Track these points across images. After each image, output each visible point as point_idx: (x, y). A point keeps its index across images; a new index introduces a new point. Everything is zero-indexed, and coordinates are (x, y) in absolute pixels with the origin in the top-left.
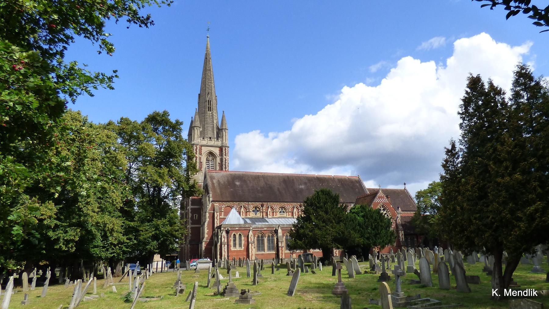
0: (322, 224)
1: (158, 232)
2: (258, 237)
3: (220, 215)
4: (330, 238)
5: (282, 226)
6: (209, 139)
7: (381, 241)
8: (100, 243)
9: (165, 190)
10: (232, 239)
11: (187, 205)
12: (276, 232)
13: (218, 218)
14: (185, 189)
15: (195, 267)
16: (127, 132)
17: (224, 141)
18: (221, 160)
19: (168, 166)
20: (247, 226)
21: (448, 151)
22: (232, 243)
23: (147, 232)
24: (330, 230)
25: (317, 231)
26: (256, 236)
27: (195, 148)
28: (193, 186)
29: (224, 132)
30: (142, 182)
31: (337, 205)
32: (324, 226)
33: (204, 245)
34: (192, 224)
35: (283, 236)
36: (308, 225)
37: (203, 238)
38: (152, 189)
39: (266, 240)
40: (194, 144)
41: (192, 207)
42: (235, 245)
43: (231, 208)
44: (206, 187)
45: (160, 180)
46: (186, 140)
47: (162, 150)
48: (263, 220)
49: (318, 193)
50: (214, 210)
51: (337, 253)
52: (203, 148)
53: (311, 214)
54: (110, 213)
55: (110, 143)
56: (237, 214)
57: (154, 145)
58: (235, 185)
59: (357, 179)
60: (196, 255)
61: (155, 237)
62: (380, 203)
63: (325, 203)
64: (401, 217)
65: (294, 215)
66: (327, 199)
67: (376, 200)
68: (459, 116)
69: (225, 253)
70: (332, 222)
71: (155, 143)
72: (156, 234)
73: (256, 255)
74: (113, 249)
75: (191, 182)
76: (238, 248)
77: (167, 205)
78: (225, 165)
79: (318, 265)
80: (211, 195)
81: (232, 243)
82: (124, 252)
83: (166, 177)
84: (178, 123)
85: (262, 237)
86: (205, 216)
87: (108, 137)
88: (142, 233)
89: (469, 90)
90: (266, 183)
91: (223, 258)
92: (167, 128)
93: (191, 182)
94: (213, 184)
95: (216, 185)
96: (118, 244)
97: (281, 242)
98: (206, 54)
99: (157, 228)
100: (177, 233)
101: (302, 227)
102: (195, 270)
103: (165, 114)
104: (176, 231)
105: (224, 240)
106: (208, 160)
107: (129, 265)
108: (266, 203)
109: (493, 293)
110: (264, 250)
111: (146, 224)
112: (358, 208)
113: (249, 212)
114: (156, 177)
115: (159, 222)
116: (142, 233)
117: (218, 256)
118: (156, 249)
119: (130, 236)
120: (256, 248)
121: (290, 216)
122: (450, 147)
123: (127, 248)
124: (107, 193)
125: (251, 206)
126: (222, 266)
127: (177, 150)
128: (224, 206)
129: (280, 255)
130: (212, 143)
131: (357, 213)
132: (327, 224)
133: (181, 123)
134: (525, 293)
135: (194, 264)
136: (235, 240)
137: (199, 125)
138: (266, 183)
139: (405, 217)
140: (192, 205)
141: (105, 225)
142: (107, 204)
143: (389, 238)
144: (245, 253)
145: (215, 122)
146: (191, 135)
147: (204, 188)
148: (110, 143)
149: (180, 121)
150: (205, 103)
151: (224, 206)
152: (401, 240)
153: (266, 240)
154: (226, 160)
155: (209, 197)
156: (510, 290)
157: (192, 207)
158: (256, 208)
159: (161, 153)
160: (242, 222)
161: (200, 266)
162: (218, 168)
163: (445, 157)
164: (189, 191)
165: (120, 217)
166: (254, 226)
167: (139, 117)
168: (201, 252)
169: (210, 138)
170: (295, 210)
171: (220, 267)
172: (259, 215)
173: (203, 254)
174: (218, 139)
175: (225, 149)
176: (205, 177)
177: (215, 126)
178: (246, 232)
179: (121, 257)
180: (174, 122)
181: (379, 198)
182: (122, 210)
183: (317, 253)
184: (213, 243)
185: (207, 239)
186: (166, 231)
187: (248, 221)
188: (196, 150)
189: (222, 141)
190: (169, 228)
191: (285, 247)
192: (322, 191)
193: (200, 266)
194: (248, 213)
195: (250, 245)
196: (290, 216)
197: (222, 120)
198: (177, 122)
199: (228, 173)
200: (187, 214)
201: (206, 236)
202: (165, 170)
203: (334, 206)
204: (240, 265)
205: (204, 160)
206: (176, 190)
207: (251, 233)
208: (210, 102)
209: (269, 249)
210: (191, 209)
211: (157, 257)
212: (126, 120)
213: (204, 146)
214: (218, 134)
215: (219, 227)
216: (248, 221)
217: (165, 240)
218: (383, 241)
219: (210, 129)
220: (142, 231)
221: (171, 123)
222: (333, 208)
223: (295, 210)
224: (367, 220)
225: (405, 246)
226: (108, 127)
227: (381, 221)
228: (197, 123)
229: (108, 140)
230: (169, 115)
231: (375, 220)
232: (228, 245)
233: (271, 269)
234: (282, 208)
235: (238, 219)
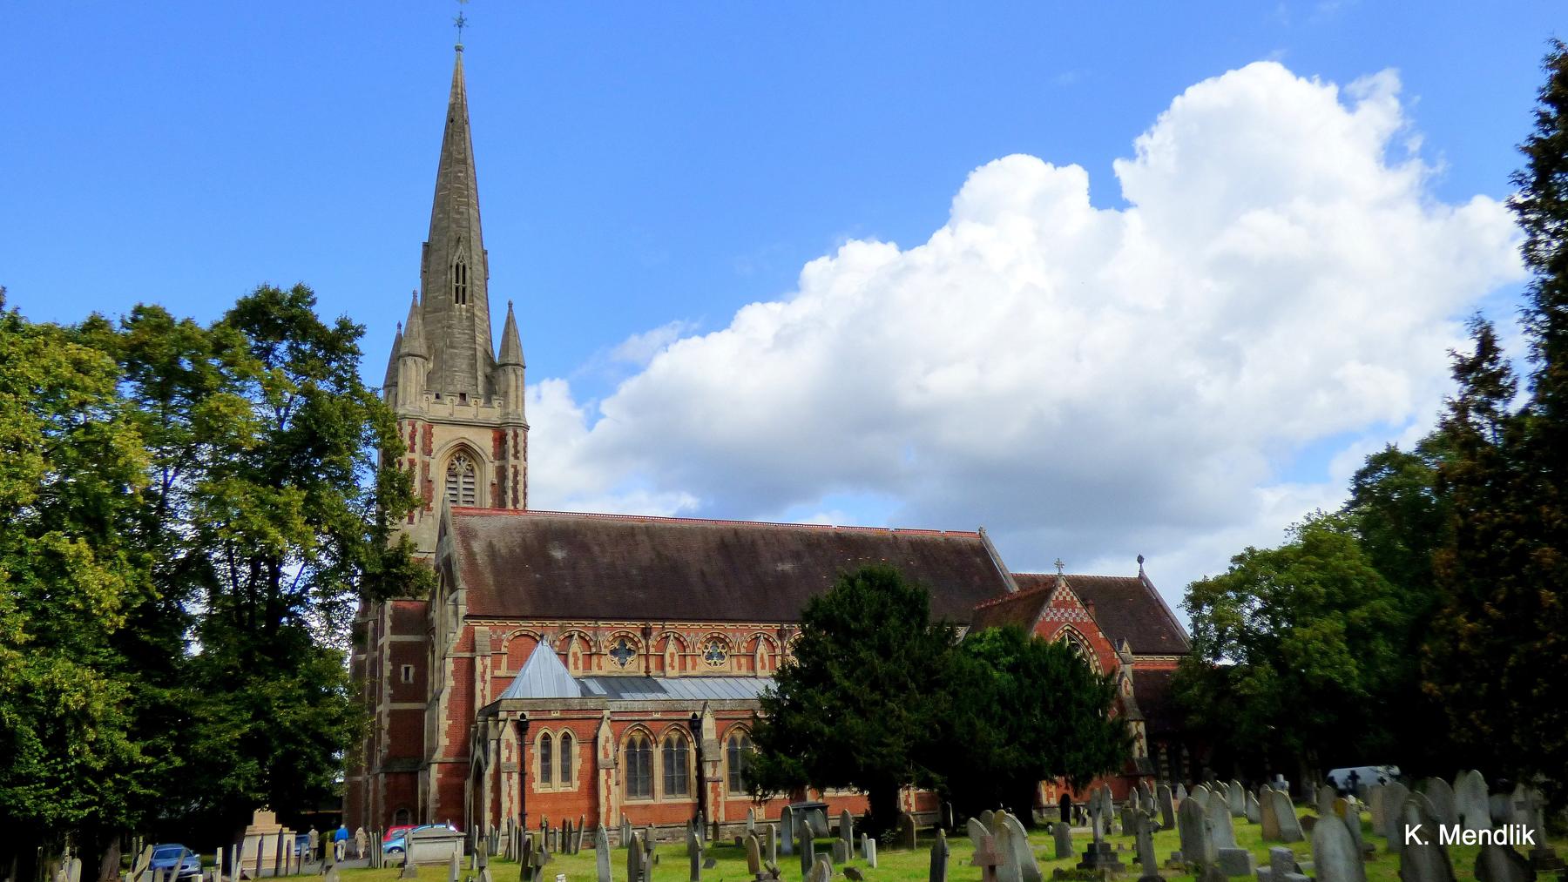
0: (866, 694)
1: (263, 724)
2: (631, 744)
4: (898, 745)
5: (717, 706)
6: (457, 400)
7: (1080, 756)
8: (35, 766)
9: (293, 572)
10: (536, 751)
11: (378, 631)
12: (695, 725)
13: (488, 677)
14: (369, 569)
15: (401, 856)
16: (155, 353)
17: (512, 407)
18: (501, 473)
19: (305, 479)
20: (591, 704)
21: (1464, 370)
22: (536, 768)
23: (222, 726)
24: (899, 718)
25: (853, 721)
26: (625, 740)
27: (407, 429)
28: (398, 558)
29: (512, 377)
30: (207, 538)
31: (921, 626)
32: (875, 703)
33: (434, 776)
34: (394, 699)
35: (720, 738)
36: (819, 698)
37: (433, 750)
38: (247, 569)
39: (658, 753)
40: (404, 417)
41: (396, 638)
42: (547, 775)
43: (536, 640)
44: (447, 565)
45: (273, 532)
46: (375, 390)
47: (286, 428)
48: (647, 683)
49: (852, 582)
50: (473, 650)
51: (912, 800)
52: (436, 430)
53: (829, 658)
54: (80, 651)
55: (85, 389)
56: (557, 661)
57: (257, 409)
58: (550, 561)
59: (975, 541)
60: (404, 808)
61: (252, 746)
62: (1059, 623)
63: (879, 618)
64: (1135, 673)
65: (759, 665)
66: (884, 605)
67: (1048, 614)
68: (1515, 215)
69: (511, 805)
70: (903, 688)
71: (258, 400)
72: (255, 731)
73: (623, 809)
74: (91, 790)
75: (393, 542)
76: (557, 785)
77: (300, 632)
78: (515, 491)
79: (858, 846)
80: (462, 595)
81: (536, 768)
82: (134, 801)
83: (298, 523)
84: (347, 331)
85: (644, 744)
86: (442, 669)
87: (79, 366)
88: (203, 730)
89: (1552, 112)
90: (659, 554)
91: (504, 820)
92: (306, 347)
93: (393, 542)
94: (470, 555)
95: (481, 559)
96: (108, 771)
97: (715, 764)
98: (452, 107)
99: (260, 709)
100: (335, 729)
101: (795, 706)
102: (402, 865)
103: (301, 295)
104: (333, 722)
105: (510, 756)
106: (452, 472)
107: (150, 848)
108: (659, 625)
109: (1408, 835)
110: (649, 791)
111: (221, 695)
112: (994, 639)
113: (599, 654)
114: (257, 521)
115: (269, 689)
116: (203, 730)
117: (488, 816)
118: (257, 790)
119: (159, 740)
120: (624, 785)
121: (744, 672)
122: (1469, 349)
123: (145, 785)
124: (64, 574)
125: (607, 632)
126: (501, 850)
127: (341, 426)
128: (509, 632)
129: (710, 809)
130: (467, 413)
131: (992, 657)
132: (885, 695)
133: (359, 332)
134: (1500, 837)
135: (399, 843)
136: (546, 758)
137: (424, 351)
138: (659, 554)
139: (1146, 674)
140: (394, 630)
141: (54, 693)
142: (70, 619)
143: (1106, 747)
144: (584, 803)
145: (480, 339)
146: (396, 384)
147: (437, 569)
148: (85, 389)
149: (355, 323)
150: (450, 270)
151: (508, 635)
152: (1136, 754)
153: (658, 753)
154: (516, 474)
155: (455, 601)
156: (1457, 828)
157: (396, 638)
158: (623, 639)
159: (279, 436)
160: (573, 691)
161: (420, 851)
162: (489, 501)
163: (1456, 390)
164: (389, 577)
165: (120, 668)
166: (615, 706)
167: (203, 304)
168: (424, 801)
169: (463, 396)
170: (762, 649)
171: (492, 854)
172: (634, 666)
173: (432, 806)
174: (489, 401)
175: (516, 435)
176: (443, 531)
177: (480, 355)
178: (588, 727)
179: (123, 819)
180: (332, 327)
181: (1058, 605)
182: (121, 640)
183: (848, 801)
184: (467, 769)
185: (446, 754)
186: (293, 722)
187: (596, 688)
188: (412, 437)
189: (506, 406)
190: (305, 711)
191: (726, 779)
192: (868, 577)
193: (420, 851)
194: (595, 659)
195: (602, 773)
196: (744, 672)
197: (506, 334)
198: (344, 326)
199: (523, 518)
200: (376, 664)
201: (444, 741)
202: (292, 495)
203: (910, 630)
204: (565, 848)
205: (439, 472)
206: (334, 571)
207: (605, 731)
208: (461, 271)
209: (670, 788)
210: (393, 645)
211: (264, 820)
212: (155, 313)
213: (436, 419)
214: (490, 381)
215: (492, 711)
216: (596, 688)
217: (292, 756)
218: (1087, 759)
219: (463, 364)
220: (204, 721)
221: (323, 329)
222: (906, 637)
223: (762, 649)
224: (1027, 682)
225: (1150, 776)
226: (87, 337)
227: (1079, 685)
228: (419, 346)
229: (79, 379)
230: (313, 302)
231: (1057, 682)
232: (522, 775)
233: (688, 862)
234: (717, 640)
235: (561, 681)
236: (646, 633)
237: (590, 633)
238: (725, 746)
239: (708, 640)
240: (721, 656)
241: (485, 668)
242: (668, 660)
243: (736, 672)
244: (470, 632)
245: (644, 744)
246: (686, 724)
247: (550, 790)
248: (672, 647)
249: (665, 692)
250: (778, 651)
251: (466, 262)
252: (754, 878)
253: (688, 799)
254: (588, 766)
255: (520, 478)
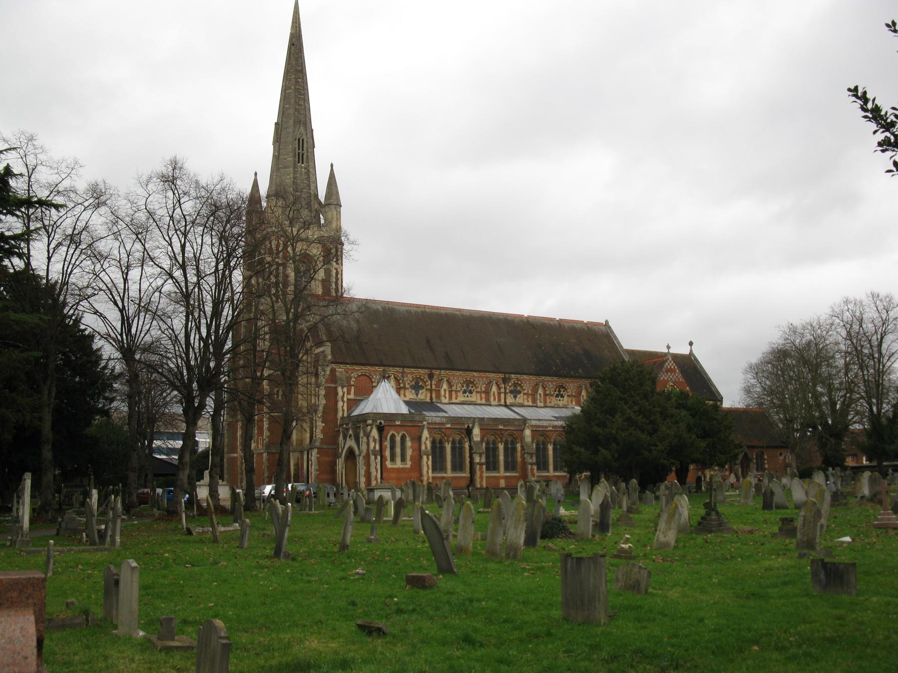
3: (349, 393)
10: (387, 443)
12: (469, 432)
13: (345, 399)
22: (387, 453)
39: (448, 447)
42: (393, 459)
62: (667, 381)
65: (492, 398)
76: (399, 464)
81: (387, 453)
105: (374, 446)
110: (443, 469)
121: (483, 402)
136: (393, 448)
151: (354, 375)
153: (448, 447)
154: (337, 274)
170: (494, 389)
181: (668, 371)
196: (483, 402)
207: (426, 434)
209: (454, 469)
223: (494, 389)
236: (431, 377)
237: (400, 375)
238: (484, 445)
239: (464, 382)
240: (471, 392)
241: (344, 393)
242: (442, 393)
243: (479, 402)
244: (333, 371)
245: (441, 442)
246: (464, 431)
247: (395, 466)
248: (445, 386)
249: (446, 412)
250: (502, 390)
251: (304, 137)
252: (892, 532)
253: (467, 474)
254: (417, 453)
255: (339, 276)
